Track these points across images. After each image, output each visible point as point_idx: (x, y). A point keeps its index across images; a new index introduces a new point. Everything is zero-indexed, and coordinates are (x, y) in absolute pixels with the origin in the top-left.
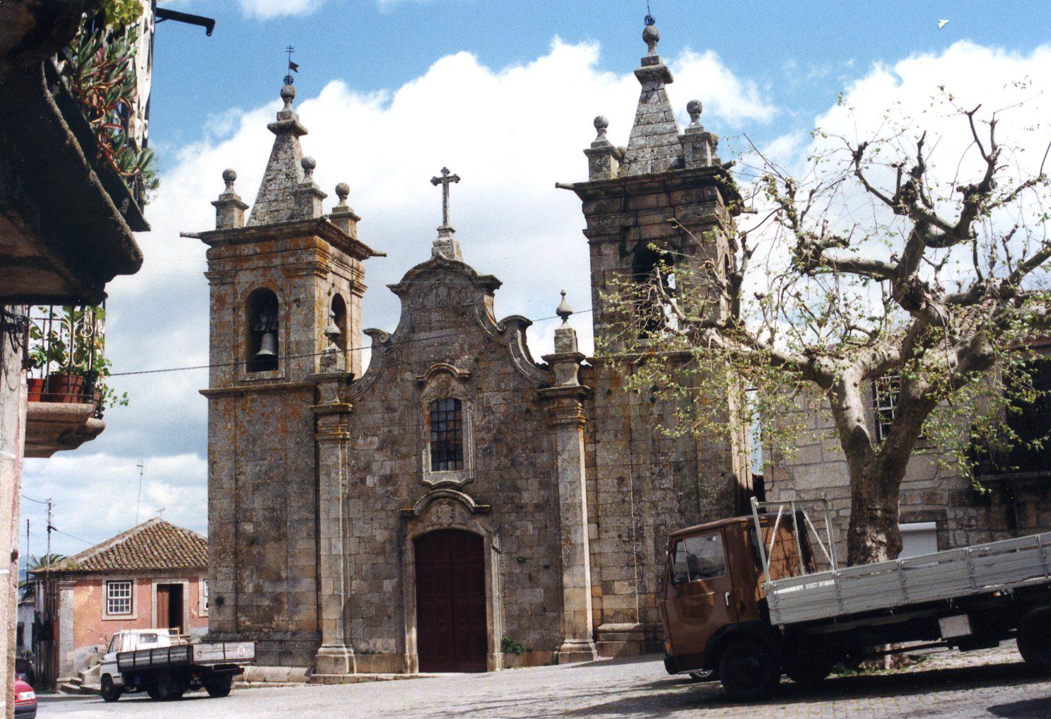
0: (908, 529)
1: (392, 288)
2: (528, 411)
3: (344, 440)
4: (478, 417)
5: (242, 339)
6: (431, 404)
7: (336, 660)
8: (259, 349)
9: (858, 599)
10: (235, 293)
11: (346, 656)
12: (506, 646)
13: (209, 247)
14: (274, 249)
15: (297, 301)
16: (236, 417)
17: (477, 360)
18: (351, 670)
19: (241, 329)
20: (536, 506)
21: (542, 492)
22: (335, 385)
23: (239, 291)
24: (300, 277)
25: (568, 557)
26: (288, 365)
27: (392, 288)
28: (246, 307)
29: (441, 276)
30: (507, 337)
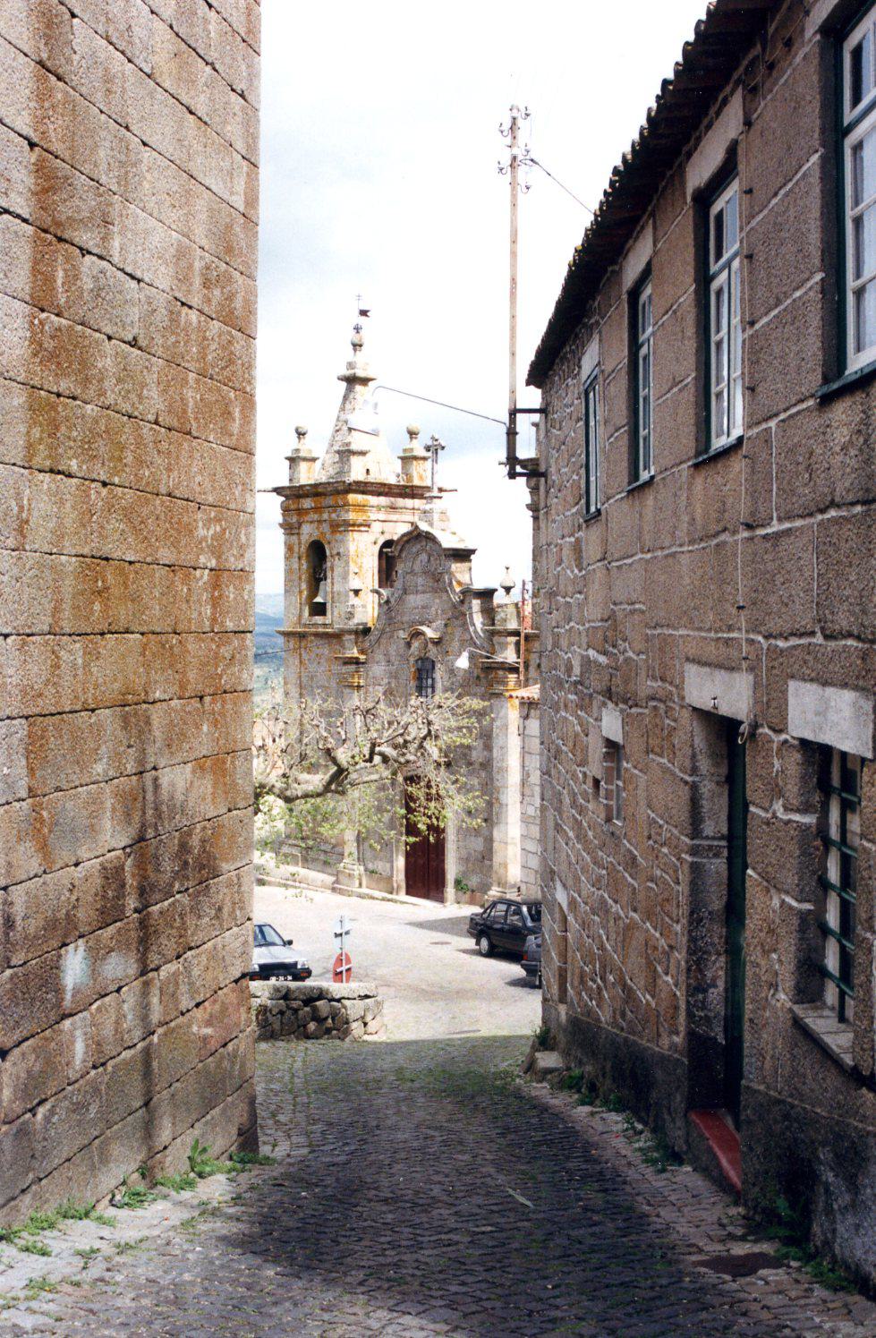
0: (848, 332)
1: (473, 552)
2: (478, 677)
3: (359, 687)
4: (446, 677)
5: (304, 586)
6: (417, 661)
7: (350, 875)
8: (316, 596)
9: (715, 825)
10: (300, 543)
11: (356, 873)
12: (458, 883)
13: (283, 499)
14: (323, 505)
15: (338, 554)
16: (300, 654)
17: (446, 625)
18: (360, 885)
19: (303, 577)
20: (481, 764)
21: (485, 753)
22: (353, 637)
23: (303, 541)
24: (341, 532)
25: (497, 814)
26: (332, 613)
27: (473, 552)
28: (307, 556)
29: (424, 543)
30: (466, 605)
